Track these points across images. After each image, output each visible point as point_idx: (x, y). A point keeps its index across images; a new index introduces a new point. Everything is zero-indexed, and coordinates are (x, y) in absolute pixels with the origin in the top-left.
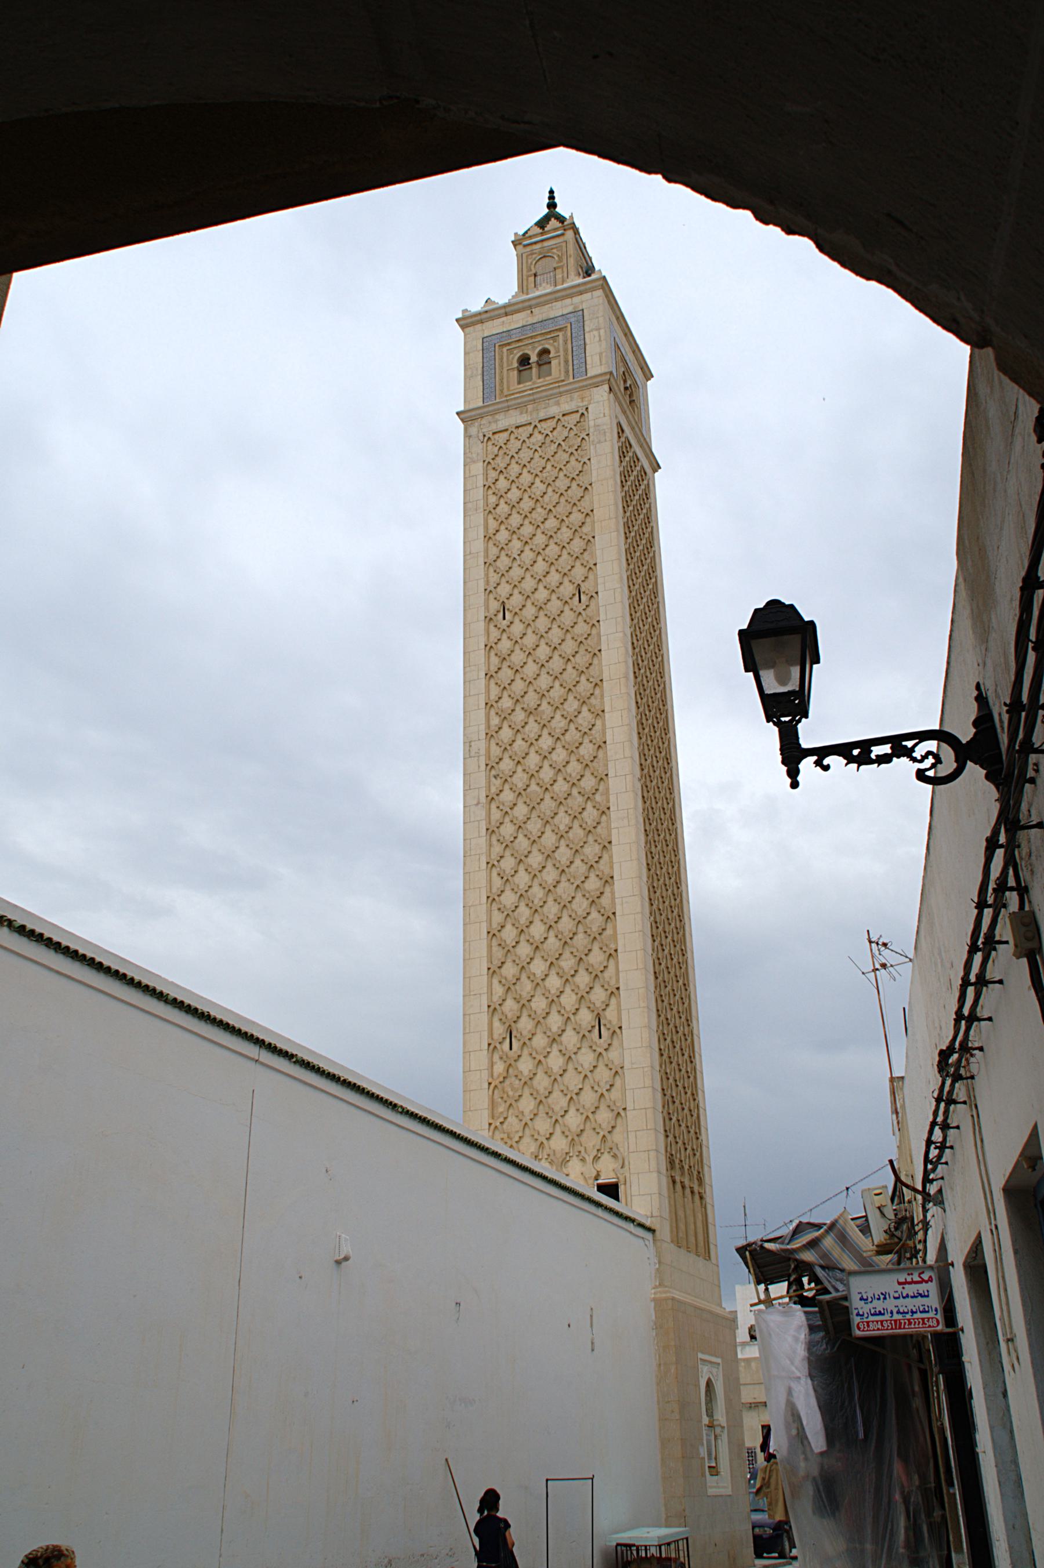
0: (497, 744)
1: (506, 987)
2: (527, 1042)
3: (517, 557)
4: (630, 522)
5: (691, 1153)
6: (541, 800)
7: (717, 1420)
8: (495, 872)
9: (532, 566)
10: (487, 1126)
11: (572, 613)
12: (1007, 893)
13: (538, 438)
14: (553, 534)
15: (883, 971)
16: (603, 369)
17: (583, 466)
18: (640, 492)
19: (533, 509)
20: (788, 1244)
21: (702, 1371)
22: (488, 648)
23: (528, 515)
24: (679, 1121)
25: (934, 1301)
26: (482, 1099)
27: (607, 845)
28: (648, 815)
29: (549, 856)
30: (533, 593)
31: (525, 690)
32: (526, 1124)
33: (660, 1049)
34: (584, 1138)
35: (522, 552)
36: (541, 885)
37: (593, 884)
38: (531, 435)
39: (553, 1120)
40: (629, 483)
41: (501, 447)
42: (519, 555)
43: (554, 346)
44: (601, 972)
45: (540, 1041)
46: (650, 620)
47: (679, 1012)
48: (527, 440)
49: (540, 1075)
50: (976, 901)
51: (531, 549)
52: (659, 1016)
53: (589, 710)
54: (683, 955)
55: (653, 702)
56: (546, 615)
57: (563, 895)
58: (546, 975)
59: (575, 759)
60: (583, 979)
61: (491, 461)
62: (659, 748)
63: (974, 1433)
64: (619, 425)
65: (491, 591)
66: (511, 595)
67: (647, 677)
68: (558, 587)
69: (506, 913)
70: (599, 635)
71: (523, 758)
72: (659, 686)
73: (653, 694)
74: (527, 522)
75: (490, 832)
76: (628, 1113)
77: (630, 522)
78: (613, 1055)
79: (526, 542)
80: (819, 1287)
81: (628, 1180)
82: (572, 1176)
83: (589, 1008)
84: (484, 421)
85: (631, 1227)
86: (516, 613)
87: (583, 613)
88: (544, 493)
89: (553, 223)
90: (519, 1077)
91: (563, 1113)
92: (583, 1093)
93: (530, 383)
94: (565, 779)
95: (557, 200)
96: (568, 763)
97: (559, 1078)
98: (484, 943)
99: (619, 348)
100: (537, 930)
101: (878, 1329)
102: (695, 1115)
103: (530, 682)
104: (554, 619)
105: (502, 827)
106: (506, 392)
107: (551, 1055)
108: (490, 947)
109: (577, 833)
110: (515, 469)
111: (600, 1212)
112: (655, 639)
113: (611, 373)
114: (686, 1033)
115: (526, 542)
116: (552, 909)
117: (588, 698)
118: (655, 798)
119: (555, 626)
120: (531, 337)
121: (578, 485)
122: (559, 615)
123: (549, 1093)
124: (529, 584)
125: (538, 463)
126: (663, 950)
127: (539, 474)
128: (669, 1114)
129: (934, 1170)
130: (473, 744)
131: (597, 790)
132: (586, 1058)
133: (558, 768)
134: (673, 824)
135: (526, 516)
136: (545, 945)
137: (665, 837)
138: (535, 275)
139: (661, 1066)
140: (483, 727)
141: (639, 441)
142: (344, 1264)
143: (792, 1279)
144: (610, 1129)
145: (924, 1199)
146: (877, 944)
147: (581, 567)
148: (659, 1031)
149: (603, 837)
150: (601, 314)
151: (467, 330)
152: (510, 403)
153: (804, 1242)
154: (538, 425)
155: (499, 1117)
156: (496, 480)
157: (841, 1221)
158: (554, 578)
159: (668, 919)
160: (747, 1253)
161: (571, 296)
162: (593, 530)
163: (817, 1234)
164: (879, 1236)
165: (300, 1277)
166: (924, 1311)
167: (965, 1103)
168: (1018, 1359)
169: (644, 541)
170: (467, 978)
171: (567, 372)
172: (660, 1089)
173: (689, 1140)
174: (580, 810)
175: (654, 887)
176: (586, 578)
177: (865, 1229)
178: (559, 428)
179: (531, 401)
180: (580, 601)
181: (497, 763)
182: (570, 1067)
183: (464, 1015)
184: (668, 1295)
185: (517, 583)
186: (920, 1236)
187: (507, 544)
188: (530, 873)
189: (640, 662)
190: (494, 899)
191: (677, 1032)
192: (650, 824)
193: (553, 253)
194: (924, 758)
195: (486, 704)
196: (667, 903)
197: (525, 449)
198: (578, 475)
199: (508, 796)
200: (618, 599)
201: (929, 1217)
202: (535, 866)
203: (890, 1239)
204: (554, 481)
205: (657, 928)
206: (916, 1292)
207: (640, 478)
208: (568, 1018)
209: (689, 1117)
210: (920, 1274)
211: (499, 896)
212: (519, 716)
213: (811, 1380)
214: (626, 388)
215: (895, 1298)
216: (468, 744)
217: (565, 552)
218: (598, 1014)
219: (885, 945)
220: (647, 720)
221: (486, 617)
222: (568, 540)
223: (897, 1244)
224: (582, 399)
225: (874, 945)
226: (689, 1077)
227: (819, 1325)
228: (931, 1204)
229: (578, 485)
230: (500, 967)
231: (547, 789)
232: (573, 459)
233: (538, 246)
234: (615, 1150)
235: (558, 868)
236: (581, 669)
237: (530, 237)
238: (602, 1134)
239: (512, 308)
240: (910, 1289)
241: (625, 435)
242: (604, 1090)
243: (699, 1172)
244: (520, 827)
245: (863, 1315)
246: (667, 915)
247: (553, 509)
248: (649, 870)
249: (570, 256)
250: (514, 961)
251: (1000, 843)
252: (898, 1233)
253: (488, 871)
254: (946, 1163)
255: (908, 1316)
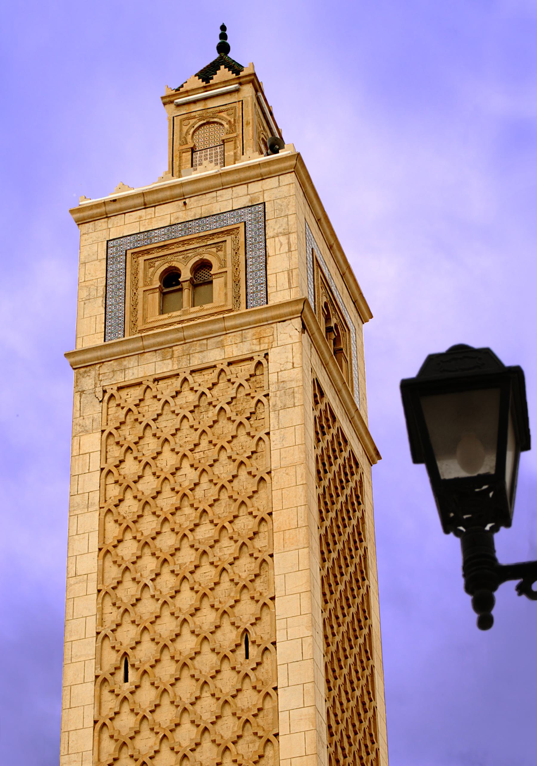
3: (150, 584)
4: (330, 536)
14: (208, 549)
17: (257, 444)
18: (347, 491)
22: (99, 725)
23: (170, 517)
30: (172, 640)
35: (157, 575)
38: (178, 393)
41: (130, 410)
42: (153, 580)
43: (219, 258)
46: (358, 693)
48: (170, 400)
51: (173, 572)
61: (114, 432)
64: (316, 384)
65: (106, 636)
66: (138, 643)
70: (276, 711)
74: (166, 528)
77: (330, 536)
79: (165, 560)
84: (105, 369)
86: (145, 672)
87: (251, 674)
88: (196, 485)
89: (223, 73)
93: (178, 313)
104: (205, 683)
106: (140, 325)
112: (366, 724)
119: (206, 694)
120: (183, 242)
121: (250, 473)
122: (213, 677)
127: (189, 453)
135: (166, 519)
138: (193, 150)
141: (347, 412)
147: (249, 601)
150: (292, 210)
152: (146, 343)
154: (189, 378)
156: (121, 462)
161: (246, 182)
169: (351, 569)
171: (237, 297)
178: (223, 384)
180: (247, 657)
185: (148, 624)
197: (167, 416)
198: (249, 457)
200: (308, 654)
214: (329, 330)
217: (225, 578)
221: (97, 677)
229: (250, 473)
232: (242, 432)
233: (199, 107)
239: (155, 197)
241: (325, 401)
247: (208, 509)
249: (248, 123)
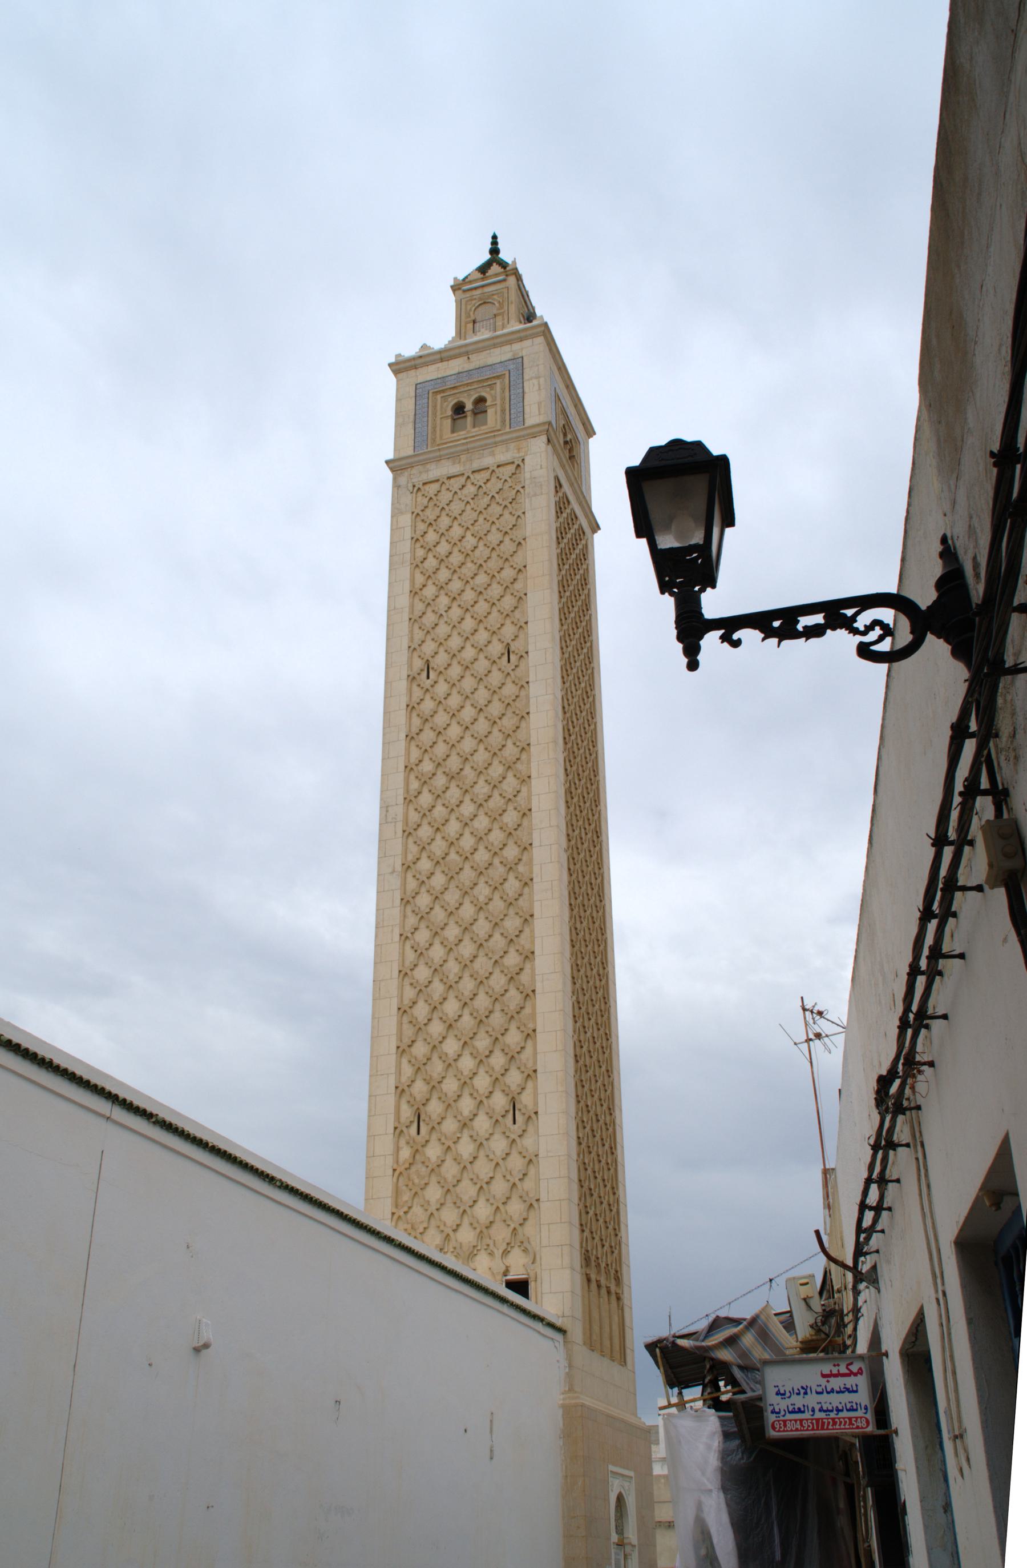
0: (416, 809)
1: (416, 1067)
2: (436, 1126)
5: (609, 1250)
6: (460, 869)
7: (628, 1538)
8: (408, 944)
9: (459, 623)
10: (390, 1216)
11: (499, 673)
12: (979, 799)
13: (471, 489)
15: (817, 1041)
16: (542, 419)
17: (517, 520)
19: (462, 564)
20: (703, 1341)
21: (613, 1485)
23: (457, 569)
24: (596, 1215)
25: (863, 1397)
26: (386, 1186)
27: (528, 918)
28: (573, 889)
29: (466, 928)
30: (459, 651)
31: (448, 753)
32: (432, 1214)
33: (579, 1138)
34: (493, 1231)
36: (457, 959)
37: (512, 960)
38: (463, 486)
39: (461, 1210)
40: (565, 541)
41: (431, 498)
42: (446, 611)
44: (518, 1053)
45: (450, 1126)
46: (583, 685)
47: (600, 1100)
48: (458, 491)
49: (449, 1161)
50: (933, 836)
51: (459, 606)
52: (579, 1102)
53: (515, 776)
54: (608, 1039)
55: (584, 771)
56: (472, 675)
57: (480, 971)
58: (459, 1056)
59: (498, 827)
60: (498, 1061)
61: (420, 513)
62: (589, 820)
63: (908, 1556)
67: (577, 744)
68: (486, 646)
69: (418, 988)
70: (528, 697)
71: (443, 825)
72: (591, 755)
73: (584, 763)
74: (455, 577)
75: (405, 902)
76: (541, 1204)
78: (528, 1142)
80: (736, 1390)
81: (538, 1277)
82: (479, 1271)
83: (503, 1091)
84: (414, 471)
85: (539, 1326)
88: (475, 548)
89: (495, 268)
90: (426, 1164)
91: (472, 1204)
92: (494, 1182)
94: (487, 848)
95: (500, 246)
96: (490, 830)
97: (468, 1166)
98: (394, 1020)
99: (559, 399)
100: (451, 1007)
101: (797, 1430)
102: (614, 1210)
103: (453, 745)
105: (418, 897)
106: (438, 441)
107: (461, 1141)
108: (400, 1024)
109: (497, 905)
110: (445, 521)
111: (505, 1308)
113: (550, 423)
114: (608, 1122)
115: (454, 598)
116: (468, 985)
117: (514, 763)
118: (583, 871)
120: (467, 385)
123: (458, 1181)
124: (455, 642)
125: (470, 515)
126: (586, 1032)
127: (470, 527)
128: (586, 1207)
129: (868, 1239)
130: (390, 809)
131: (520, 860)
132: (499, 1145)
133: (479, 836)
134: (601, 901)
135: (455, 571)
136: (459, 1024)
137: (591, 913)
138: (474, 322)
139: (579, 1155)
140: (401, 792)
141: (578, 498)
142: (204, 1352)
143: (707, 1380)
144: (522, 1222)
145: (855, 1277)
146: (812, 1012)
147: (510, 625)
148: (578, 1118)
149: (524, 909)
151: (401, 375)
152: (442, 453)
153: (721, 1339)
155: (403, 1207)
156: (425, 533)
157: (762, 1317)
158: (482, 636)
159: (592, 1000)
160: (658, 1350)
161: (510, 342)
162: (525, 586)
163: (735, 1330)
164: (803, 1330)
165: (150, 1365)
166: (851, 1409)
167: (908, 1145)
168: (968, 1460)
170: (374, 1057)
171: (503, 422)
172: (576, 1180)
173: (607, 1237)
174: (502, 881)
175: (577, 965)
176: (516, 637)
177: (789, 1325)
179: (465, 451)
181: (415, 830)
182: (482, 1154)
183: (370, 1096)
184: (578, 1401)
185: (442, 641)
186: (849, 1330)
187: (433, 600)
188: (445, 946)
189: (571, 728)
190: (406, 974)
191: (598, 1121)
192: (576, 899)
193: (494, 299)
194: (869, 628)
195: (406, 767)
196: (591, 983)
197: (456, 502)
198: (511, 529)
199: (425, 865)
201: (860, 1304)
202: (452, 939)
203: (816, 1335)
204: (485, 535)
205: (580, 1008)
206: (842, 1386)
207: (578, 537)
208: (481, 1101)
209: (608, 1212)
210: (848, 1365)
211: (412, 970)
212: (440, 781)
213: (724, 1493)
214: (566, 443)
215: (817, 1393)
216: (385, 809)
217: (495, 609)
218: (513, 1098)
219: (820, 1013)
220: (576, 789)
221: (408, 676)
222: (499, 597)
223: (824, 1340)
224: (519, 450)
225: (807, 1013)
226: (609, 1169)
227: (734, 1432)
228: (864, 1284)
229: (511, 539)
230: (409, 1046)
231: (467, 858)
234: (526, 1244)
235: (475, 942)
236: (507, 732)
237: (471, 282)
238: (512, 1226)
240: (836, 1383)
242: (517, 1179)
243: (617, 1272)
244: (437, 897)
245: (779, 1413)
246: (591, 996)
247: (483, 564)
248: (573, 946)
249: (512, 303)
250: (425, 1040)
251: (971, 730)
252: (826, 1329)
253: (402, 943)
254: (883, 1231)
255: (833, 1415)
